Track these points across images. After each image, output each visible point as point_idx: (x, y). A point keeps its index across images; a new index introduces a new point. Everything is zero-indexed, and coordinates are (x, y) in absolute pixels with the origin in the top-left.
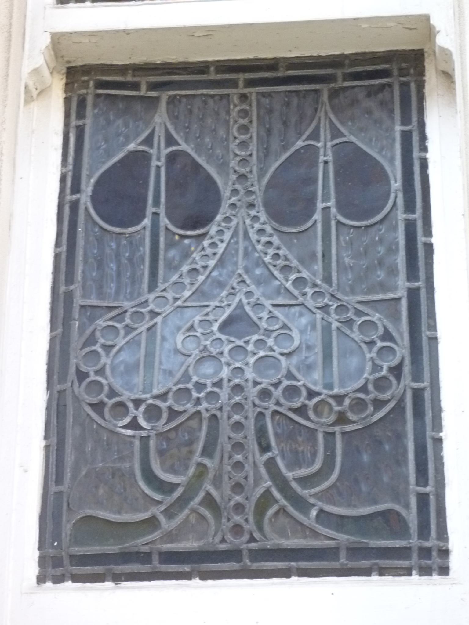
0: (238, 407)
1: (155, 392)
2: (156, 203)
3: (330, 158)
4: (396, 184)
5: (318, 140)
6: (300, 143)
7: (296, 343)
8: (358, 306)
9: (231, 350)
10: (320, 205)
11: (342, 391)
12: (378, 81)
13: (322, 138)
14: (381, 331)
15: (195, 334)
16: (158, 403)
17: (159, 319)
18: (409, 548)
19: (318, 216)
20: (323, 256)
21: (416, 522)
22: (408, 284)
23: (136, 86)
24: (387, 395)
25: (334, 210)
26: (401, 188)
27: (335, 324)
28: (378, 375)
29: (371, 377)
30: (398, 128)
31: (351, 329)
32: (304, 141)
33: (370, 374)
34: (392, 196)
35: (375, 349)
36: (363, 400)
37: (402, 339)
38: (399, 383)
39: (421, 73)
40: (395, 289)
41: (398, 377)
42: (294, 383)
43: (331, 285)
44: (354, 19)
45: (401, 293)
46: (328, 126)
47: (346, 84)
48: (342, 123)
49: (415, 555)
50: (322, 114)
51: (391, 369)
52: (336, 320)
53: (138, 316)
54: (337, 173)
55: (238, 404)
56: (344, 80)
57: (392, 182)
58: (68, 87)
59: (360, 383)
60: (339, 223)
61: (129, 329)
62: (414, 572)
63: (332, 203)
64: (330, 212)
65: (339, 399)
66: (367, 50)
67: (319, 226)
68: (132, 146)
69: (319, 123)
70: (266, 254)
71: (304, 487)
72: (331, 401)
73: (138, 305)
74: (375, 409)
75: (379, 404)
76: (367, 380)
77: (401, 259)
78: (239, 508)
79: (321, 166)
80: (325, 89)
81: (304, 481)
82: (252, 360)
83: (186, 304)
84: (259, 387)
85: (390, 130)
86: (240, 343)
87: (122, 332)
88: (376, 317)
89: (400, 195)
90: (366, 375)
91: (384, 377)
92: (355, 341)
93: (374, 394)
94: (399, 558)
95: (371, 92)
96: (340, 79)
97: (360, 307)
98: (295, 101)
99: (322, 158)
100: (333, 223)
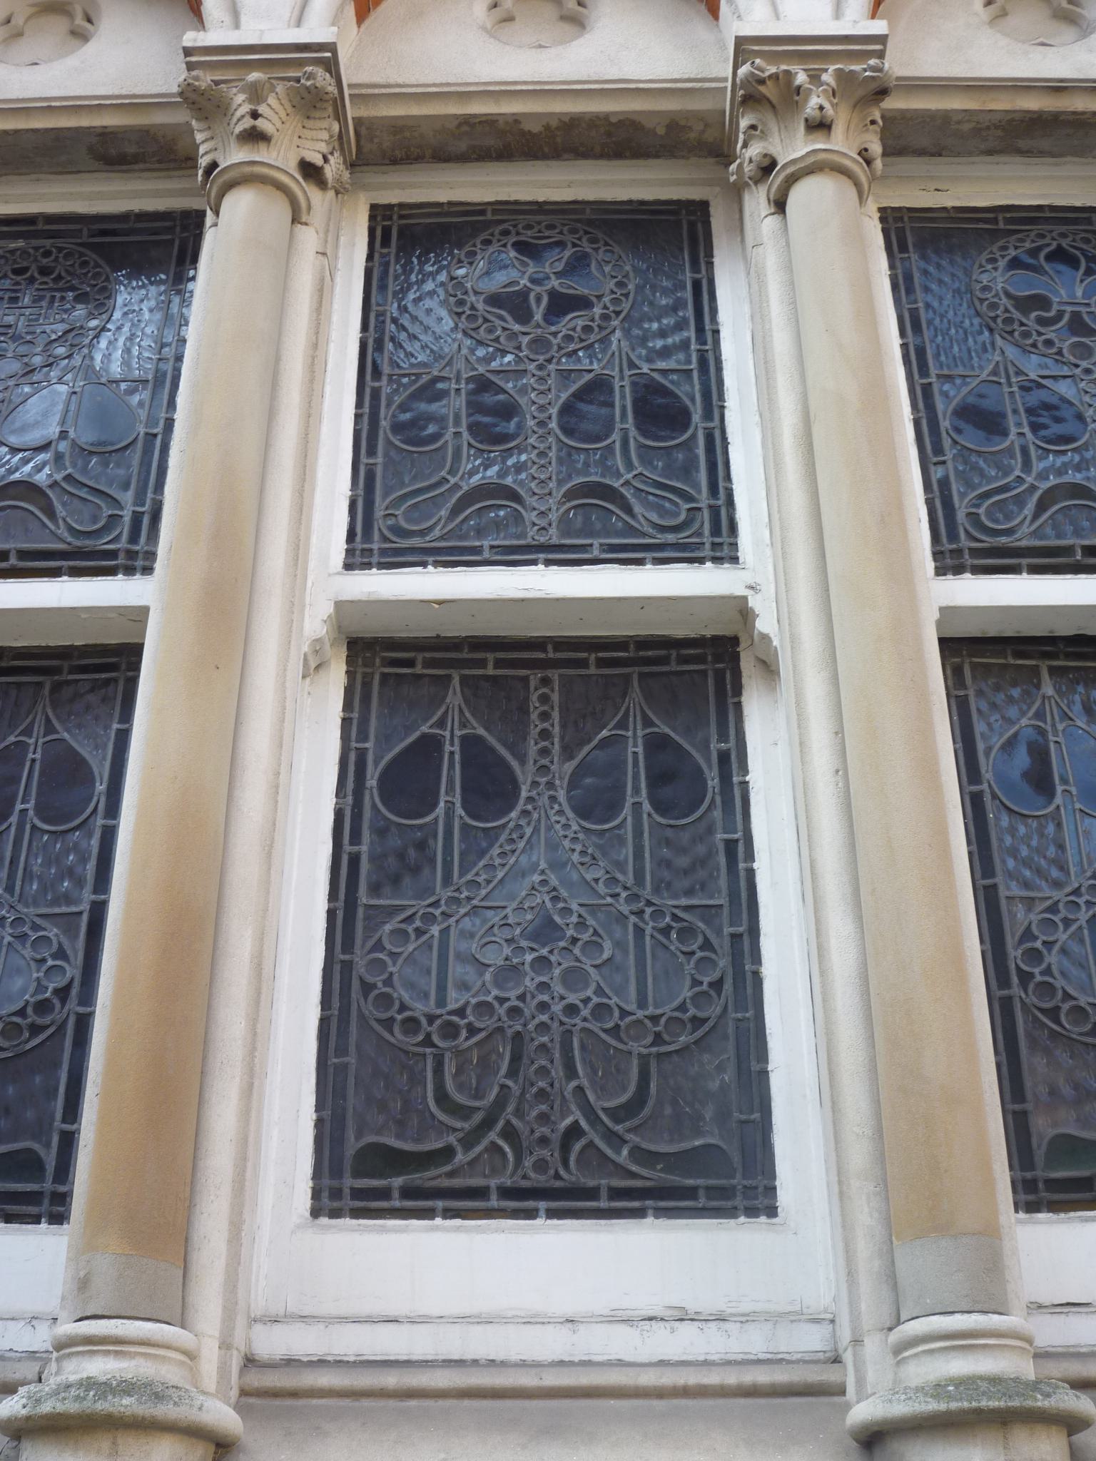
0: (543, 1027)
1: (452, 1006)
2: (636, 791)
3: (38, 756)
4: (101, 787)
5: (627, 729)
6: (12, 739)
7: (606, 956)
8: (38, 921)
9: (534, 960)
10: (19, 806)
11: (659, 1012)
12: (104, 676)
13: (35, 734)
14: (55, 946)
15: (493, 939)
16: (455, 1018)
17: (453, 920)
18: (41, 1193)
19: (627, 810)
20: (11, 862)
21: (54, 1164)
22: (93, 897)
23: (410, 663)
24: (47, 1020)
25: (31, 813)
26: (105, 791)
27: (648, 931)
28: (40, 997)
29: (32, 1000)
30: (115, 726)
31: (24, 946)
32: (610, 730)
33: (32, 996)
34: (95, 799)
35: (44, 968)
36: (17, 1024)
37: (76, 959)
38: (62, 1008)
39: (736, 658)
40: (77, 902)
41: (64, 1001)
42: (605, 1000)
43: (12, 896)
44: (422, 601)
45: (85, 907)
46: (43, 721)
47: (70, 677)
48: (58, 718)
49: (46, 1201)
50: (40, 709)
51: (711, 985)
52: (10, 935)
53: (429, 918)
54: (42, 774)
55: (543, 1024)
56: (70, 673)
57: (98, 784)
58: (350, 661)
59: (20, 1005)
60: (34, 827)
61: (419, 932)
62: (43, 1220)
63: (30, 805)
64: (26, 815)
65: (655, 1019)
66: (98, 642)
67: (13, 829)
68: (425, 729)
69: (34, 719)
70: (573, 850)
71: (617, 1121)
72: (647, 1021)
73: (429, 906)
74: (30, 1035)
75: (35, 1029)
76: (27, 1002)
77: (91, 866)
78: (544, 1141)
79: (28, 764)
80: (48, 682)
81: (614, 1114)
82: (557, 972)
83: (483, 904)
84: (564, 1002)
85: (107, 727)
86: (544, 952)
87: (413, 936)
88: (53, 932)
89: (103, 799)
90: (27, 997)
91: (47, 1000)
92: (25, 958)
93: (32, 1017)
94: (29, 1204)
95: (95, 687)
96: (66, 670)
97: (38, 921)
98: (13, 693)
99: (31, 756)
100: (28, 827)
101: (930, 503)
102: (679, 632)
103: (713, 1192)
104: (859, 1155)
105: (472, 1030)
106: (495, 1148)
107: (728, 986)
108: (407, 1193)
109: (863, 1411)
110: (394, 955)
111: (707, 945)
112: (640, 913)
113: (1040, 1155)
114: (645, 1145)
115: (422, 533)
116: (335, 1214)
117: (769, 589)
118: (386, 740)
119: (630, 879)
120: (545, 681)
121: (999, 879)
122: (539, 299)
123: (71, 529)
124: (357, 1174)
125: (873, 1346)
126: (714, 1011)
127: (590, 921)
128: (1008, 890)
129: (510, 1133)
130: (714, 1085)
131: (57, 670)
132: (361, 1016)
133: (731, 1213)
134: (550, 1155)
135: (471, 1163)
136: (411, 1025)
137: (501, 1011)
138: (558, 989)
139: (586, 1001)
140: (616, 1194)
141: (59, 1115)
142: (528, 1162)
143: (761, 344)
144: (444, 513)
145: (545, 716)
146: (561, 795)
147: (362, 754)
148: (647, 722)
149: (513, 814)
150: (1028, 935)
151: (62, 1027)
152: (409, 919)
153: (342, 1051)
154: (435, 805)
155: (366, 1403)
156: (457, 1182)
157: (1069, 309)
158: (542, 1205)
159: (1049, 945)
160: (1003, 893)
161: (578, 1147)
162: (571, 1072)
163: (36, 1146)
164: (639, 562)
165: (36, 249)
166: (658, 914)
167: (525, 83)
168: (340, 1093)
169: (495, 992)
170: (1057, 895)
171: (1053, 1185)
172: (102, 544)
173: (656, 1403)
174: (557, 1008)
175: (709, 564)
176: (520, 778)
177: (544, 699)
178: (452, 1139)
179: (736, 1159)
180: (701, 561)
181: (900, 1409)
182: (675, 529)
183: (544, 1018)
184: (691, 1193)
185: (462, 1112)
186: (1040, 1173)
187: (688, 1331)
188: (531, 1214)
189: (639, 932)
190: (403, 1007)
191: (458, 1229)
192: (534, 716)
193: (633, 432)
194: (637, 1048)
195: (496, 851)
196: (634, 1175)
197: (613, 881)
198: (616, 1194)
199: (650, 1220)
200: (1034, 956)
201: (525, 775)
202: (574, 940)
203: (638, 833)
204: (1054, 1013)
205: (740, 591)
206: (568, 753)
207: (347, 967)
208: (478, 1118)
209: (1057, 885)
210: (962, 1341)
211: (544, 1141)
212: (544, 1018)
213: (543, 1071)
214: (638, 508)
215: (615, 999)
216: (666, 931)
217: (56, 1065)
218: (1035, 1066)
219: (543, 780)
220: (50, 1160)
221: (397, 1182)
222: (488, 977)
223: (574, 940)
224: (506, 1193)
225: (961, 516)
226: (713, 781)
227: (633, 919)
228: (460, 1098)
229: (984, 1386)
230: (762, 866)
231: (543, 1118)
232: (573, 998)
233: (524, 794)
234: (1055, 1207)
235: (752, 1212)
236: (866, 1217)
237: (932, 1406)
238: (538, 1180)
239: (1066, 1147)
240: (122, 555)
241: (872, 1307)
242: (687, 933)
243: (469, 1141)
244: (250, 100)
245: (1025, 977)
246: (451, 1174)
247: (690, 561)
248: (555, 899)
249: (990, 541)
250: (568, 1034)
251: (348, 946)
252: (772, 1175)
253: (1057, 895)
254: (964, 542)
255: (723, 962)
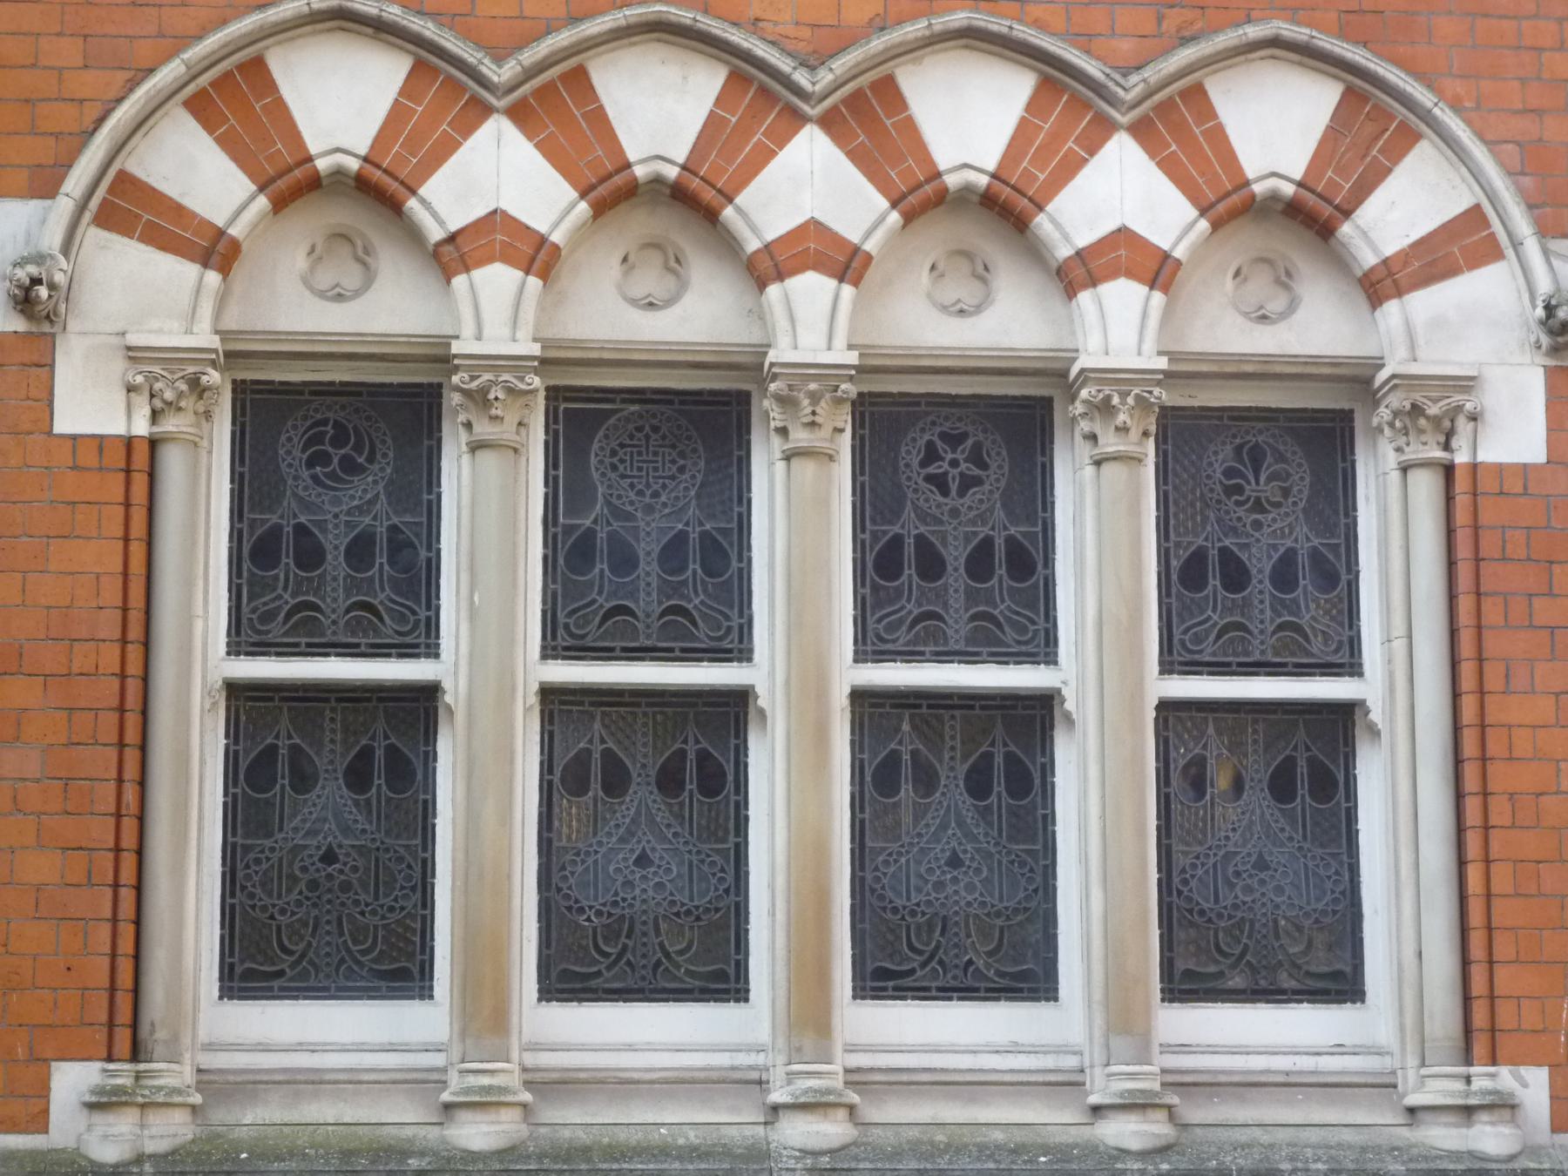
0: (956, 913)
1: (914, 901)
27: (1004, 862)
45: (730, 845)
78: (956, 966)
82: (962, 884)
88: (716, 858)
101: (1160, 629)
102: (1023, 693)
103: (1030, 990)
104: (1098, 995)
105: (924, 914)
106: (934, 969)
107: (1041, 892)
108: (895, 989)
109: (1094, 1099)
110: (885, 874)
111: (1031, 870)
112: (1000, 853)
113: (1177, 977)
114: (1002, 969)
115: (894, 641)
116: (863, 998)
117: (1073, 684)
118: (874, 754)
119: (995, 833)
120: (953, 717)
121: (1174, 841)
122: (954, 479)
123: (708, 636)
124: (873, 980)
125: (1098, 1071)
126: (1033, 904)
127: (977, 857)
128: (1177, 847)
129: (941, 962)
130: (1033, 940)
131: (695, 705)
132: (871, 905)
133: (1037, 999)
134: (959, 973)
135: (924, 976)
136: (895, 910)
137: (937, 904)
138: (963, 893)
139: (975, 899)
140: (988, 990)
141: (733, 952)
142: (949, 976)
143: (1078, 521)
144: (904, 628)
145: (953, 738)
146: (961, 784)
147: (862, 761)
148: (1005, 745)
149: (937, 795)
150: (1183, 871)
151: (729, 908)
152: (890, 854)
153: (862, 921)
154: (899, 791)
155: (895, 1087)
156: (917, 984)
157: (1254, 494)
158: (955, 995)
159: (1193, 876)
160: (1174, 848)
161: (971, 969)
162: (969, 936)
163: (725, 967)
164: (1007, 663)
165: (647, 412)
166: (1009, 853)
167: (955, 349)
168: (863, 941)
169: (934, 895)
170: (1198, 849)
171: (1181, 991)
172: (725, 644)
173: (1010, 1088)
174: (963, 903)
175: (1042, 666)
176: (940, 773)
177: (952, 727)
178: (915, 965)
179: (1041, 973)
180: (1039, 663)
181: (1107, 1101)
182: (1026, 643)
183: (957, 908)
184: (1021, 990)
185: (920, 953)
186: (1176, 986)
187: (1022, 1057)
188: (950, 999)
189: (1000, 863)
190: (891, 902)
191: (919, 1006)
192: (947, 738)
193: (1005, 577)
194: (999, 922)
195: (930, 815)
196: (995, 982)
197: (986, 835)
198: (988, 990)
199: (1002, 1003)
200: (1185, 882)
201: (943, 773)
202: (969, 867)
203: (1000, 807)
204: (1190, 911)
205: (1058, 685)
206: (965, 757)
207: (863, 879)
208: (926, 955)
209: (1201, 844)
210: (1132, 1076)
211: (956, 966)
212: (957, 898)
213: (956, 934)
214: (1007, 629)
215: (989, 899)
216: (1012, 862)
217: (729, 927)
218: (1180, 935)
219: (952, 775)
220: (731, 971)
221: (891, 984)
222: (930, 886)
223: (969, 867)
224: (939, 989)
225: (1175, 641)
226: (1037, 782)
227: (997, 856)
228: (917, 945)
229: (1138, 1094)
230: (1060, 829)
231: (957, 956)
232: (969, 898)
233: (943, 783)
234: (1181, 1001)
235: (1048, 1000)
236: (1099, 1021)
237: (1119, 1101)
238: (953, 983)
239: (1189, 974)
240: (735, 651)
241: (1099, 1057)
242: (1023, 864)
243: (924, 965)
244: (810, 404)
245: (1180, 893)
246: (915, 981)
247: (1033, 663)
248: (960, 844)
249: (1189, 657)
250: (967, 916)
251: (862, 868)
252: (1056, 981)
253: (1198, 849)
254: (1176, 657)
255: (1039, 879)
